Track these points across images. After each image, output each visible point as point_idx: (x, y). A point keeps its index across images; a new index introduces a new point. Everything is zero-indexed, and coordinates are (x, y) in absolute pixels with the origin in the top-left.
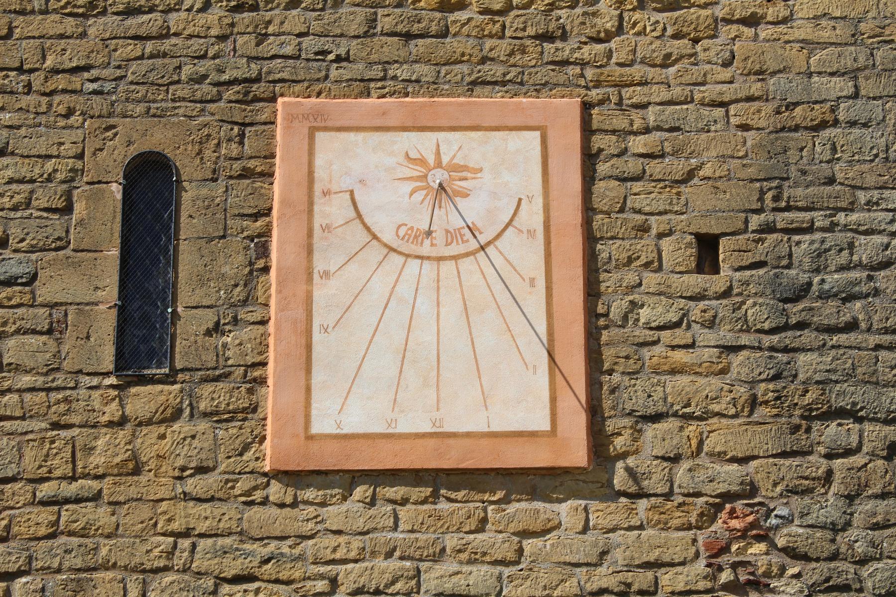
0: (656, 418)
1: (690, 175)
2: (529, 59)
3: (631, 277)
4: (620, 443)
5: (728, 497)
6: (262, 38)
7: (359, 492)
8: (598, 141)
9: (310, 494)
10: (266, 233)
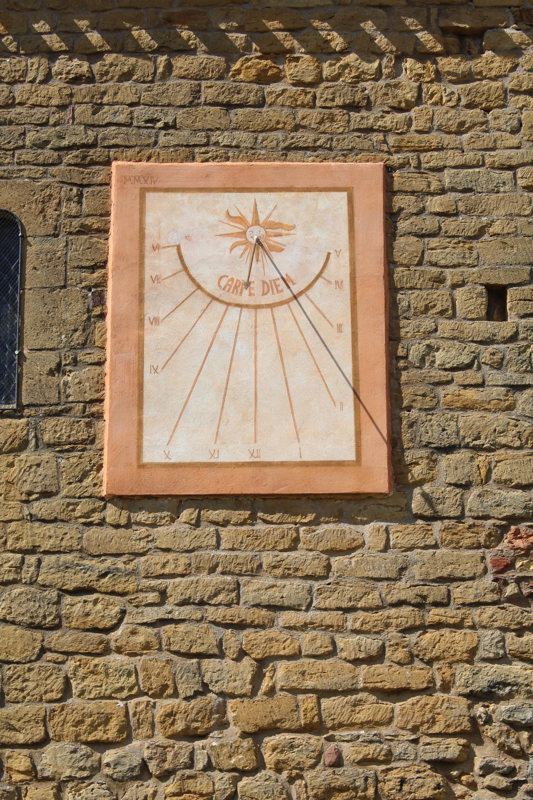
0: (450, 449)
1: (481, 232)
2: (338, 126)
3: (427, 324)
4: (417, 472)
5: (513, 519)
6: (98, 107)
7: (186, 514)
8: (399, 201)
9: (142, 516)
10: (102, 283)
